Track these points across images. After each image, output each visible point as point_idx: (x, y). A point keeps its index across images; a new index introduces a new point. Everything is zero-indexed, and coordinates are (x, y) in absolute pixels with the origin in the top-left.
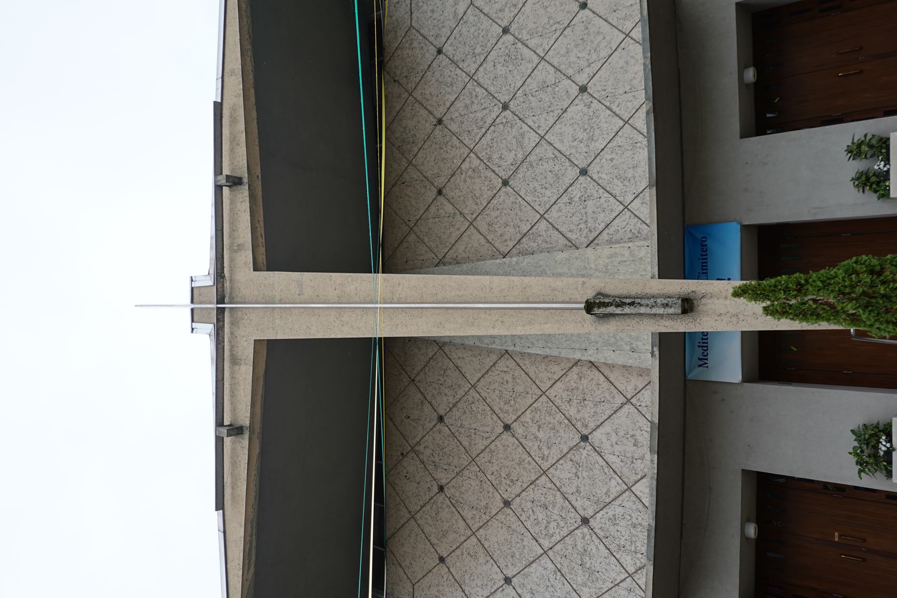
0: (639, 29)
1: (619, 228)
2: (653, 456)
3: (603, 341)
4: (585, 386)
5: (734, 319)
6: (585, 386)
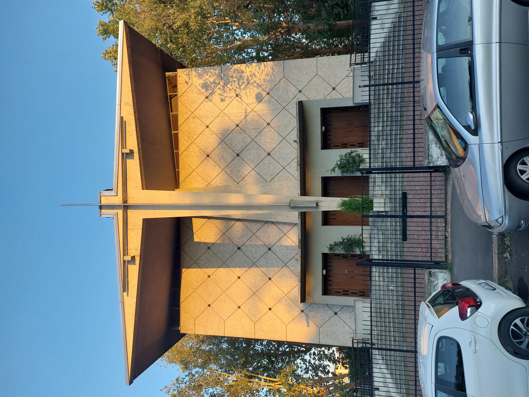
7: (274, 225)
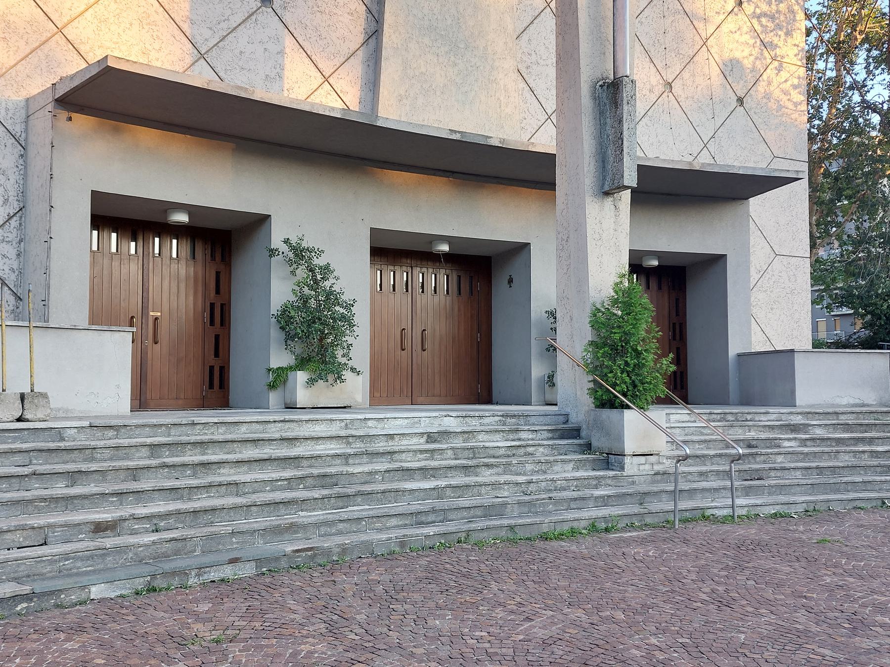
0: (710, 161)
1: (528, 105)
2: (339, 111)
3: (409, 59)
4: (341, 18)
5: (597, 236)
6: (341, 18)
7: (361, 39)
